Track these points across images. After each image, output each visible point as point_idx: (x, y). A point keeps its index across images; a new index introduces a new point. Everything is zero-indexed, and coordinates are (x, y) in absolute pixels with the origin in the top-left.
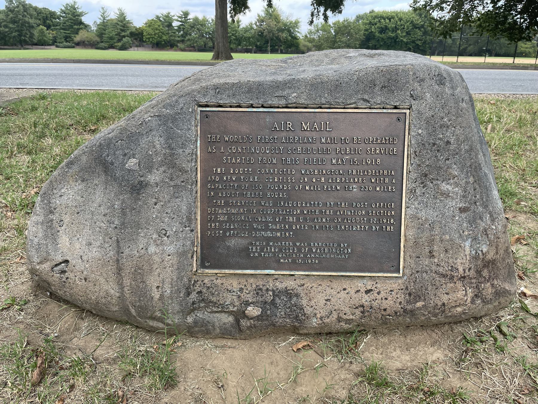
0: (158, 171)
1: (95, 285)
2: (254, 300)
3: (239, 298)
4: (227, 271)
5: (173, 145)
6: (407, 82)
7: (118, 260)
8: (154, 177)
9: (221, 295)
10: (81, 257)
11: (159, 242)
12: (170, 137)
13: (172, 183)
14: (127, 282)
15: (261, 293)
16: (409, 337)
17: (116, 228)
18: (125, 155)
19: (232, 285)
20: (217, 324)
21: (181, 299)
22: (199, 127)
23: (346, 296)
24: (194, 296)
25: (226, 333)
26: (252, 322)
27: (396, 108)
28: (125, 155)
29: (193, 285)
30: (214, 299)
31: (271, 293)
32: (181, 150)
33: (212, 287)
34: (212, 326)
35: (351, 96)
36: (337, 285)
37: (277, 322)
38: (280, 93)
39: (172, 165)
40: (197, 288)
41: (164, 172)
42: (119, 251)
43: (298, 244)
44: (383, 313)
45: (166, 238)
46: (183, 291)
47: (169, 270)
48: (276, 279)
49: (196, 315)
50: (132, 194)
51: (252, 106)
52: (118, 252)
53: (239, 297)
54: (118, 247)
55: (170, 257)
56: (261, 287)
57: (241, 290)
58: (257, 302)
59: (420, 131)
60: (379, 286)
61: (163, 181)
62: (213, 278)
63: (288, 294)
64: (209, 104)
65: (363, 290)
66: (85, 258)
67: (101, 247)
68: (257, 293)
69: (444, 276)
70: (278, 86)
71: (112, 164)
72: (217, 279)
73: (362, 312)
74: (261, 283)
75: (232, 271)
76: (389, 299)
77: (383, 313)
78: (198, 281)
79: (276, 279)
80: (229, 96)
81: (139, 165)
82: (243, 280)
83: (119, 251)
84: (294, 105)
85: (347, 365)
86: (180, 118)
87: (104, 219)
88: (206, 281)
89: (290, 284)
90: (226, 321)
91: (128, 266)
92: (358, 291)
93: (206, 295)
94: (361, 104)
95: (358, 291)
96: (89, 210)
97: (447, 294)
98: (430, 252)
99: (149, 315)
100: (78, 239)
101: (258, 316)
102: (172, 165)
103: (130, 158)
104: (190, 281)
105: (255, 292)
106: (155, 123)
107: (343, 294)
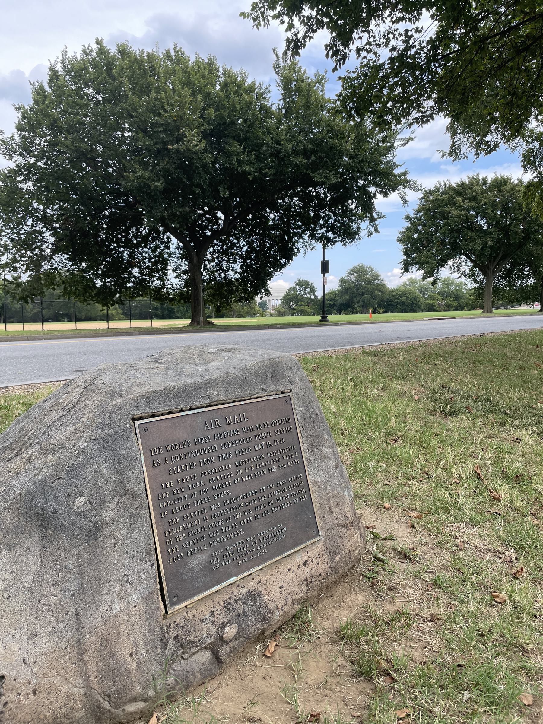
0: (111, 503)
1: (49, 693)
2: (229, 618)
3: (213, 623)
4: (196, 598)
5: (121, 468)
6: (284, 371)
7: (79, 641)
8: (108, 514)
9: (197, 629)
10: (24, 660)
11: (123, 594)
12: (116, 460)
13: (127, 514)
14: (92, 666)
15: (231, 608)
16: (334, 596)
17: (73, 595)
18: (69, 495)
19: (202, 612)
20: (196, 669)
21: (159, 656)
22: (140, 442)
23: (292, 575)
24: (171, 644)
25: (209, 675)
26: (232, 646)
27: (282, 393)
28: (69, 495)
29: (167, 632)
30: (192, 638)
31: (240, 602)
32: (130, 472)
33: (186, 625)
34: (192, 675)
35: (254, 387)
36: (283, 569)
37: (250, 633)
38: (203, 394)
39: (125, 492)
40: (173, 634)
41: (118, 502)
42: (79, 627)
43: (249, 539)
44: (320, 578)
45: (129, 586)
46: (159, 644)
47: (137, 625)
48: (238, 586)
49: (174, 670)
50: (87, 541)
51: (181, 411)
52: (78, 630)
53: (213, 622)
54: (78, 621)
55: (136, 608)
56: (229, 600)
57: (212, 613)
58: (232, 619)
59: (301, 409)
60: (310, 554)
61: (118, 515)
62: (184, 614)
63: (253, 596)
64: (143, 415)
65: (302, 564)
66: (30, 659)
67: (54, 631)
68: (229, 610)
69: (342, 526)
70: (199, 388)
71: (55, 512)
72: (187, 613)
73: (307, 586)
74: (227, 596)
75: (200, 596)
76: (320, 563)
77: (320, 578)
78: (170, 624)
79: (238, 586)
80: (160, 404)
81: (90, 503)
82: (210, 603)
83: (79, 627)
84: (216, 403)
85: (318, 642)
86: (119, 437)
87: (54, 589)
88: (178, 621)
89: (251, 585)
90: (204, 660)
91: (92, 642)
92: (299, 566)
93: (183, 637)
94: (262, 394)
95: (299, 566)
96: (24, 587)
97: (349, 541)
98: (330, 509)
99: (128, 697)
100: (14, 636)
101: (238, 633)
102: (125, 492)
103: (75, 498)
104: (162, 629)
105: (226, 609)
106: (93, 449)
107: (290, 575)
